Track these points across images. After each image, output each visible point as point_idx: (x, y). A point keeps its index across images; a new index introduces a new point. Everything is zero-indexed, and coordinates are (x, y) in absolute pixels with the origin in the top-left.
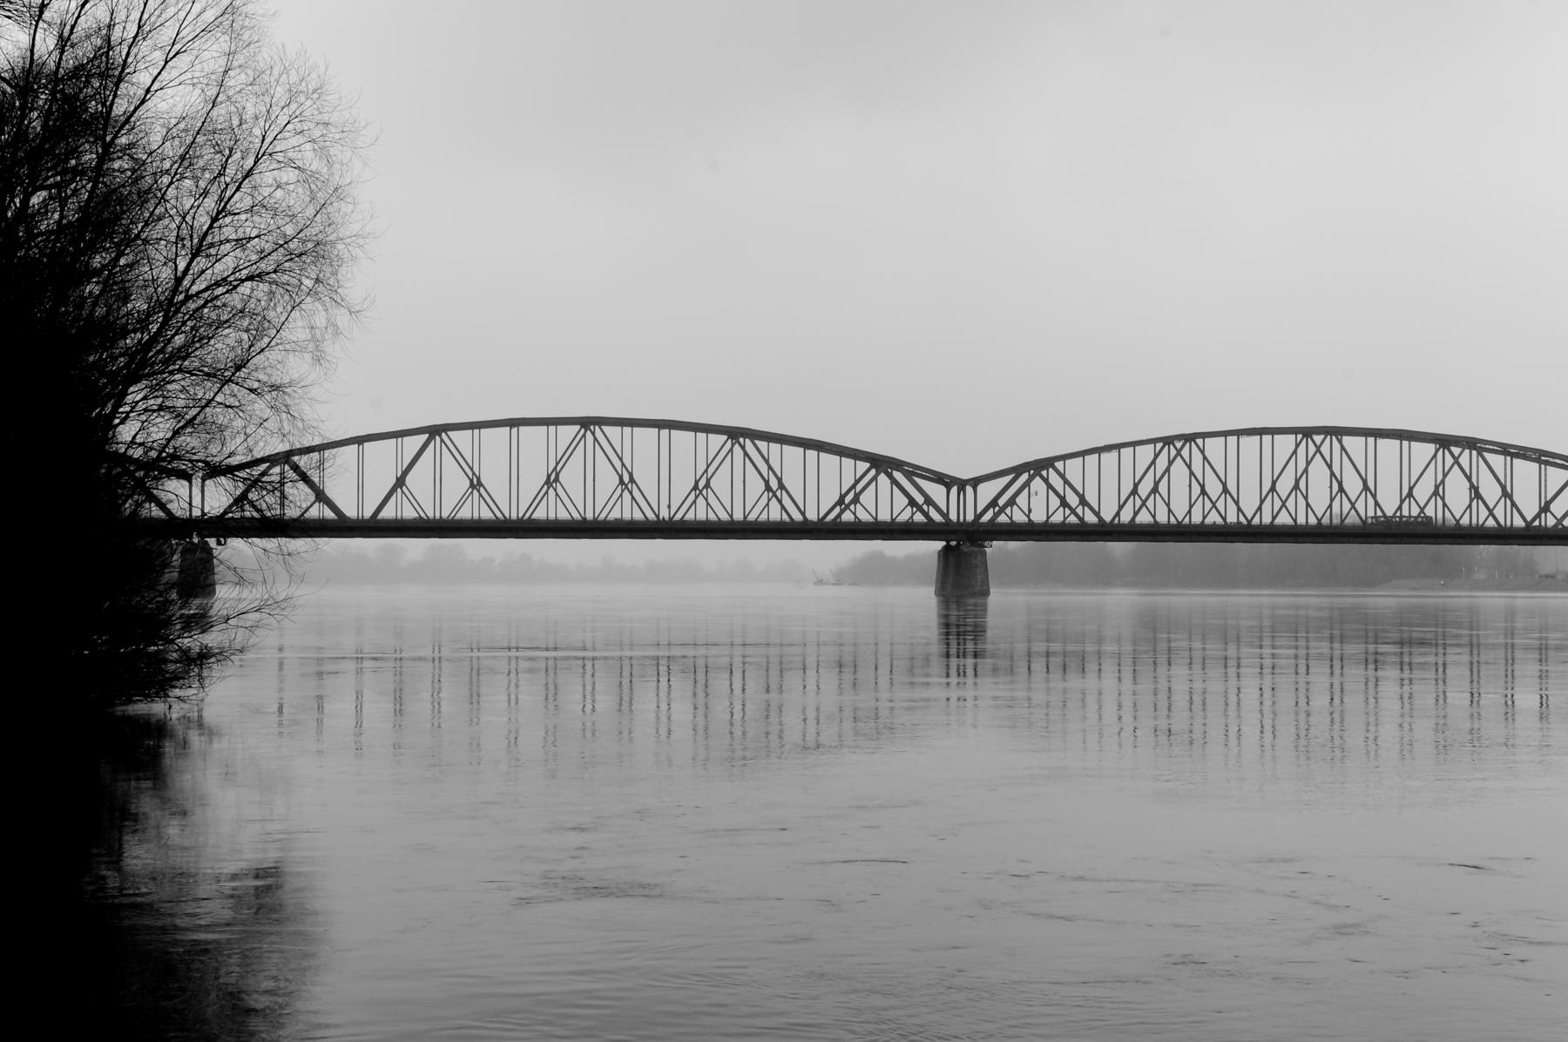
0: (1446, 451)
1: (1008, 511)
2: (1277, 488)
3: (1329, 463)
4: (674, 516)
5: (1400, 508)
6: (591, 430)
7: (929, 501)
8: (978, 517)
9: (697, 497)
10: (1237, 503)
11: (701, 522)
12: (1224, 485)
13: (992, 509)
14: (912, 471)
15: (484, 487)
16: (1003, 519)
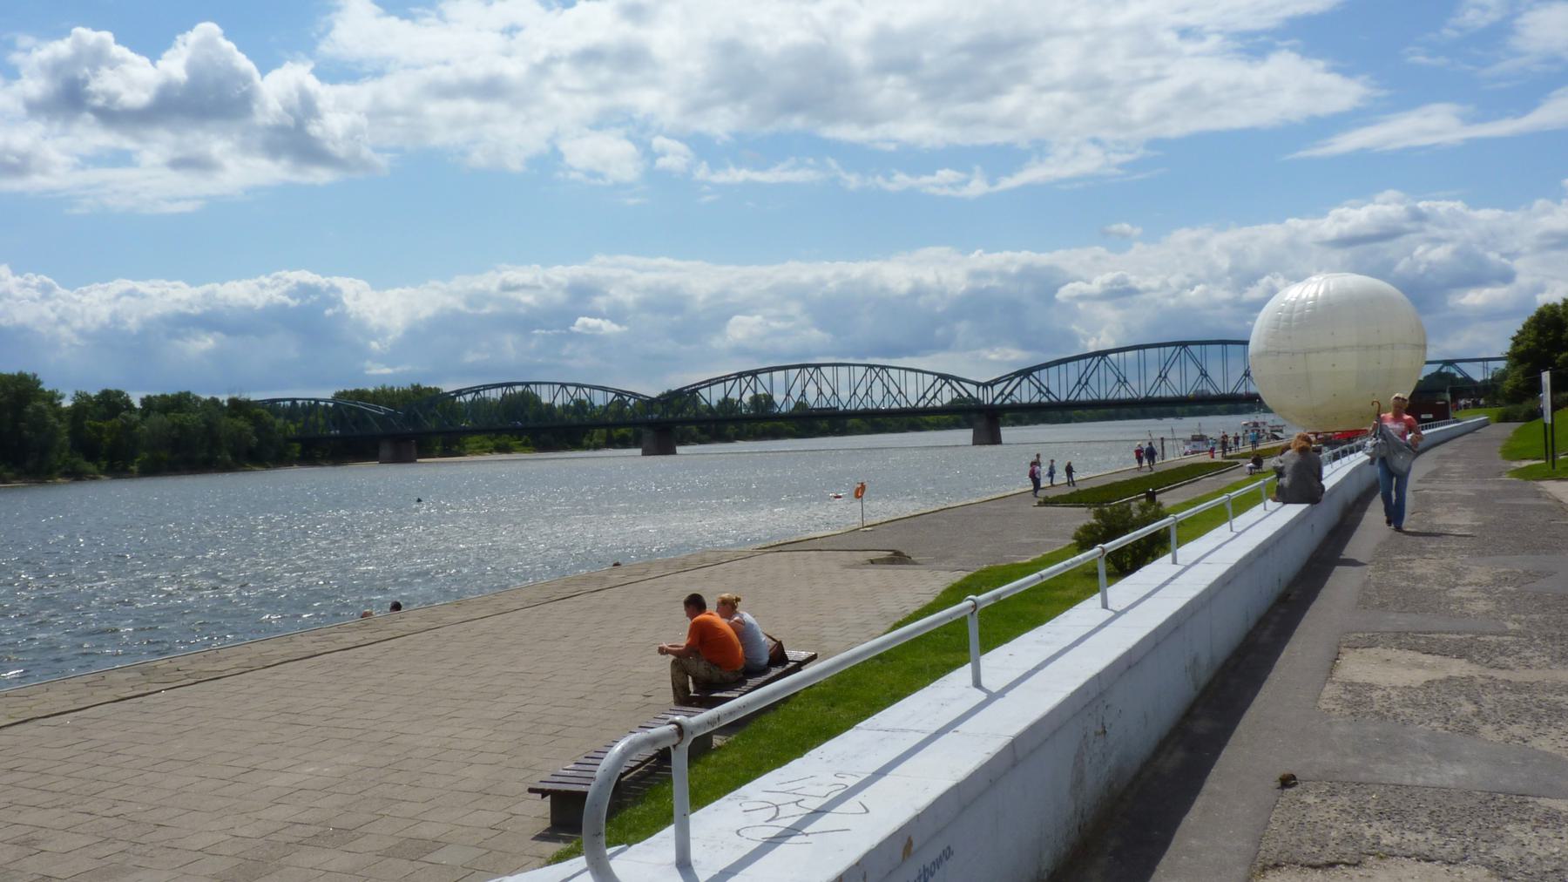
1: (933, 401)
8: (994, 400)
9: (1161, 382)
10: (905, 397)
12: (899, 389)
14: (958, 380)
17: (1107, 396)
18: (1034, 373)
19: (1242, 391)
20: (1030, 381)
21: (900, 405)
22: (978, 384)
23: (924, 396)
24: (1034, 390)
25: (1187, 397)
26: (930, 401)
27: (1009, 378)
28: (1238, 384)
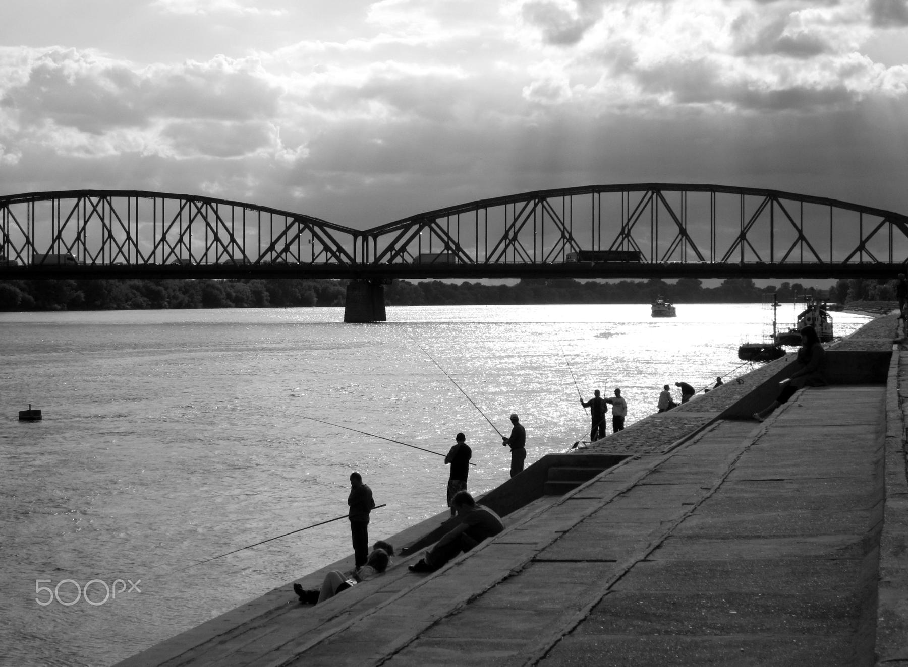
0: (208, 206)
1: (284, 256)
2: (167, 239)
3: (192, 218)
4: (546, 260)
5: (52, 247)
6: (107, 200)
7: (340, 250)
8: (377, 260)
9: (507, 247)
11: (510, 265)
12: (128, 233)
13: (390, 253)
14: (322, 224)
15: (575, 242)
16: (398, 260)
17: (164, 262)
18: (438, 220)
19: (675, 260)
20: (432, 229)
21: (128, 261)
22: (355, 234)
23: (272, 248)
24: (319, 247)
25: (544, 264)
26: (279, 256)
27: (404, 225)
28: (669, 253)
